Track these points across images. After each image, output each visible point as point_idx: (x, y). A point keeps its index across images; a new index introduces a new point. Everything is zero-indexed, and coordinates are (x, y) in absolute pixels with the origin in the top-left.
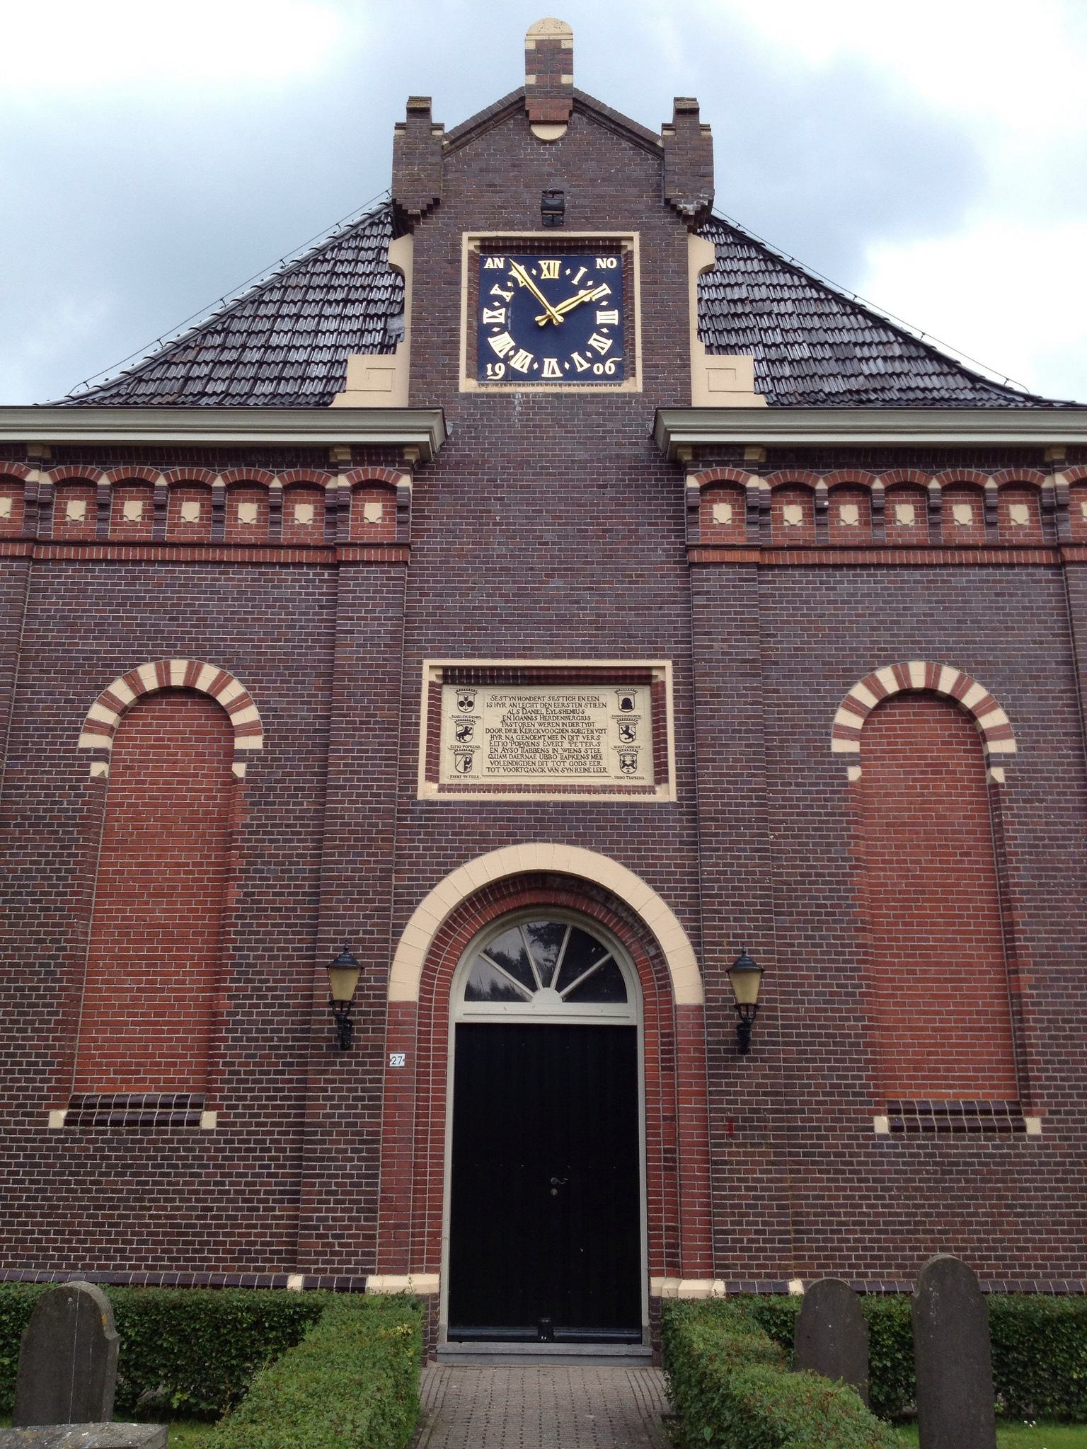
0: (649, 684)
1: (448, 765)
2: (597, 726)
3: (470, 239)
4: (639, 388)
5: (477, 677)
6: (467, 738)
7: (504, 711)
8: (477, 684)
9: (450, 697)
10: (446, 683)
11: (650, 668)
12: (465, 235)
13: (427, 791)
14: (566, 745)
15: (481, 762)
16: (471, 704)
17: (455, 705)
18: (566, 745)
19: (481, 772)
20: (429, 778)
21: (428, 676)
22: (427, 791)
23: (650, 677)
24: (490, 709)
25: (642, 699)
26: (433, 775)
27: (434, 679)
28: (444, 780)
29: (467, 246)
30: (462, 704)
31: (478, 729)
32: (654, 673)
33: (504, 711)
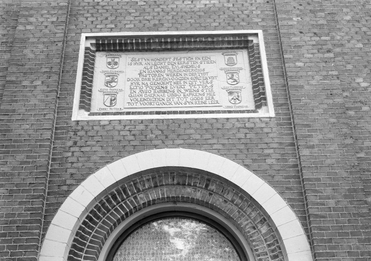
0: (246, 48)
1: (98, 101)
2: (209, 75)
3: (87, 38)
4: (272, 114)
5: (120, 44)
6: (113, 84)
7: (141, 67)
8: (121, 50)
9: (101, 60)
10: (98, 50)
11: (246, 35)
12: (84, 36)
13: (78, 115)
14: (187, 87)
15: (122, 104)
16: (116, 63)
17: (103, 83)
18: (187, 87)
19: (122, 104)
20: (81, 107)
21: (84, 44)
22: (78, 115)
23: (247, 41)
24: (129, 66)
25: (242, 58)
26: (85, 105)
27: (89, 45)
28: (94, 109)
29: (84, 44)
30: (109, 63)
31: (121, 79)
32: (250, 38)
33: (141, 67)
